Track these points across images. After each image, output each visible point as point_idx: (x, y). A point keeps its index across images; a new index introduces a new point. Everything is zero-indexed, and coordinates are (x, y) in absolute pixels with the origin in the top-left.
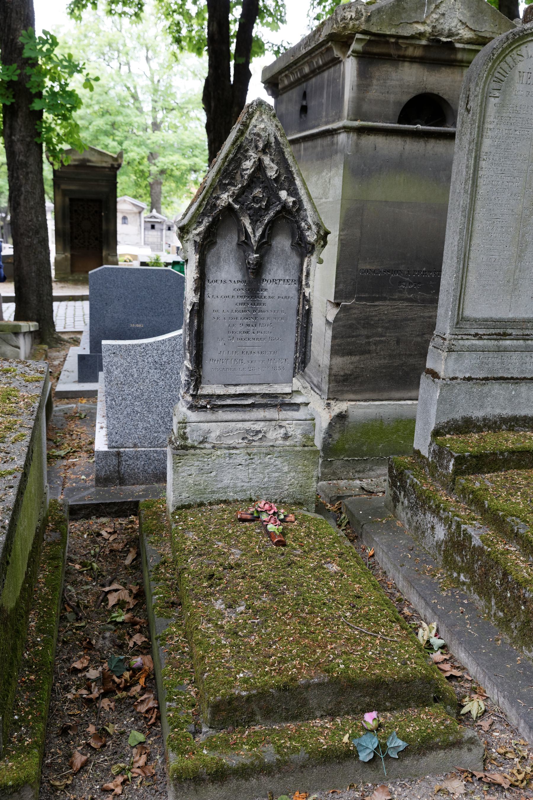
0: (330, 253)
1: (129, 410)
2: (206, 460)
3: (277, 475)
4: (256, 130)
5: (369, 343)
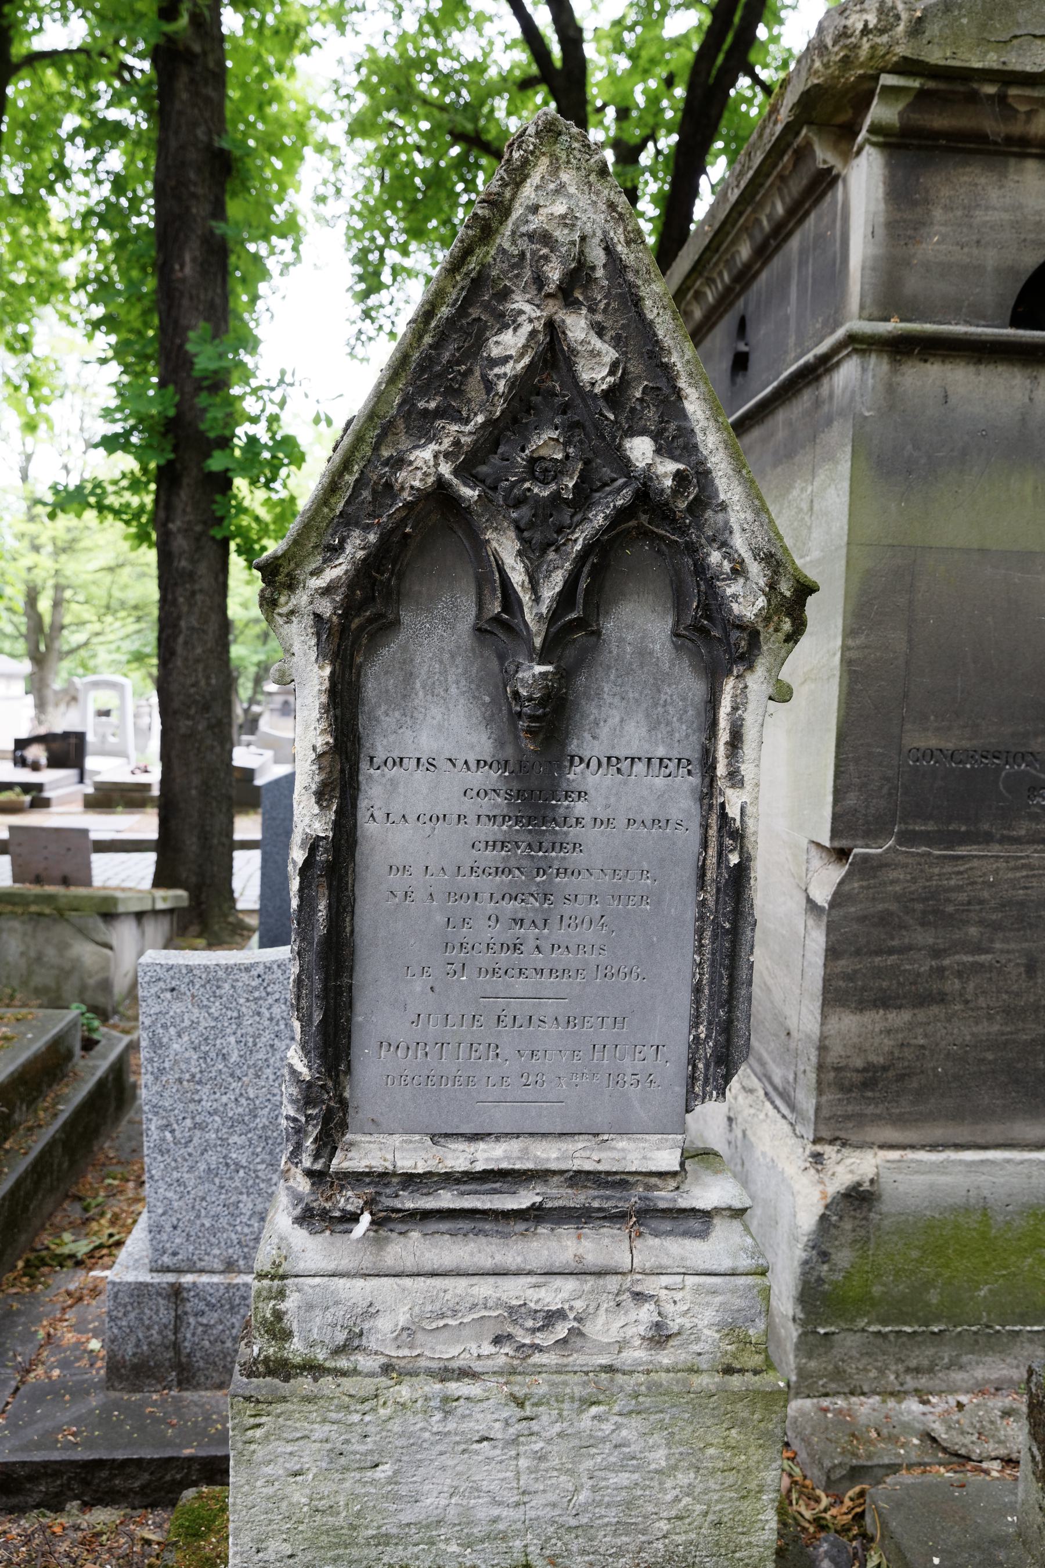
0: (816, 660)
1: (212, 1158)
2: (356, 1418)
3: (624, 1478)
4: (535, 223)
5: (941, 971)
